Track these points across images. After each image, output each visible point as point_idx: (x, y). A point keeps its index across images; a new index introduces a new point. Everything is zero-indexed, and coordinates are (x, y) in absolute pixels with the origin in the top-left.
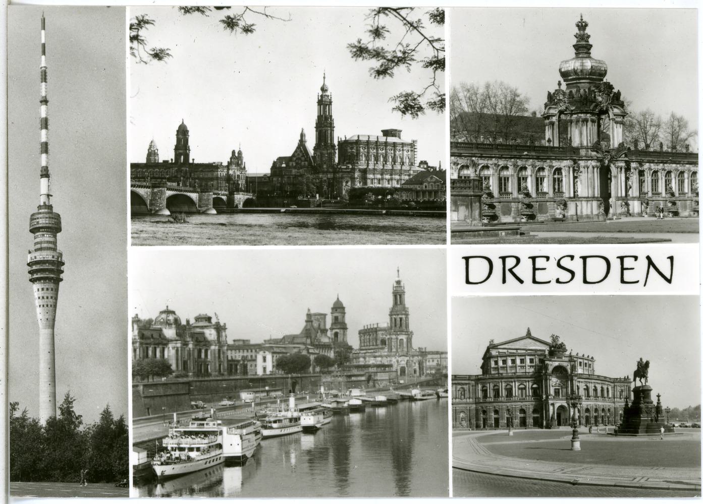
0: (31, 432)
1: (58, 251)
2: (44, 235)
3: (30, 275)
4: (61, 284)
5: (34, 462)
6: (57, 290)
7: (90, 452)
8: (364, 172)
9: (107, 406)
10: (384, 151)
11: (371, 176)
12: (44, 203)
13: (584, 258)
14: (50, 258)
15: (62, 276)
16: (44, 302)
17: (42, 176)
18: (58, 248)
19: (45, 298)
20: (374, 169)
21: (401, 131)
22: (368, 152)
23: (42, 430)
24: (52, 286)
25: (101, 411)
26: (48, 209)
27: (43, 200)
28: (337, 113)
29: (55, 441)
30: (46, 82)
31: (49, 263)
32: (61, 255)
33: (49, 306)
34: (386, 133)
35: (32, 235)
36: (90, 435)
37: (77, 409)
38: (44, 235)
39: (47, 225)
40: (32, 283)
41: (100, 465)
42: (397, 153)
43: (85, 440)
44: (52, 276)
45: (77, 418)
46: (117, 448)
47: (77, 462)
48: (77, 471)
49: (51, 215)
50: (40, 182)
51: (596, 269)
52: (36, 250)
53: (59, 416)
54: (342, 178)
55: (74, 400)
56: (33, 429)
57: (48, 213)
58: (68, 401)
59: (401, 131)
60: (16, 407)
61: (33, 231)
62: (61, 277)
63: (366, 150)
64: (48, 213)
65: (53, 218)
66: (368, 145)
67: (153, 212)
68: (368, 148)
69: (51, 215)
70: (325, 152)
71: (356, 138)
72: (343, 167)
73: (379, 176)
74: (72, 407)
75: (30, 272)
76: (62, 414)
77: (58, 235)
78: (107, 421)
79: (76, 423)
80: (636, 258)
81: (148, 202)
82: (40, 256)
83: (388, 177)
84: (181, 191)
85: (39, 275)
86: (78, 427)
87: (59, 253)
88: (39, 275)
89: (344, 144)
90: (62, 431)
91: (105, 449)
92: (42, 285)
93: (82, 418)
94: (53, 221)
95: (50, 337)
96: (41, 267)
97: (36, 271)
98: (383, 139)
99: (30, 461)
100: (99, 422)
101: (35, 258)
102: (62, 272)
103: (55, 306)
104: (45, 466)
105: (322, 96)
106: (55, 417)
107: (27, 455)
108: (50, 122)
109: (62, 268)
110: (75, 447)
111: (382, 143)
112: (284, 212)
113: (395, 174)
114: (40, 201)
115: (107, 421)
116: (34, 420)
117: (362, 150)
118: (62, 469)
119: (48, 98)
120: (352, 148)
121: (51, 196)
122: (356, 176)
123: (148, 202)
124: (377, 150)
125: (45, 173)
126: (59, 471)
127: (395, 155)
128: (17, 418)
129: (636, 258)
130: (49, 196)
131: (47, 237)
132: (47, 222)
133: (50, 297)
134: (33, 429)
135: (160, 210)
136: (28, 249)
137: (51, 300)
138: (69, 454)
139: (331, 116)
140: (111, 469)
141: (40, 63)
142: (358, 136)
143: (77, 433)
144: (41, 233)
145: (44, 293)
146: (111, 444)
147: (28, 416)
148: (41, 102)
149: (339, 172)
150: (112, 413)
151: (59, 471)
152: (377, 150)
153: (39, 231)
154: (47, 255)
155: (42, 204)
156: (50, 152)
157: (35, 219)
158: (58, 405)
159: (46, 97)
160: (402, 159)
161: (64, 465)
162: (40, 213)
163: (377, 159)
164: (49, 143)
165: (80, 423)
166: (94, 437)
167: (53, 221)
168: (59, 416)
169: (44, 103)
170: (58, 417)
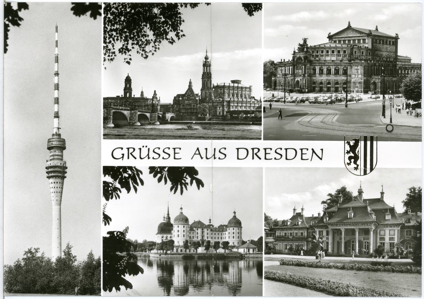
0: (47, 265)
1: (64, 161)
2: (55, 151)
3: (47, 174)
4: (65, 179)
5: (48, 282)
6: (63, 183)
7: (81, 277)
8: (229, 102)
9: (91, 251)
10: (237, 91)
11: (232, 104)
12: (56, 132)
13: (286, 149)
14: (59, 164)
15: (66, 175)
16: (56, 190)
17: (55, 117)
18: (64, 159)
19: (56, 187)
20: (234, 101)
21: (241, 81)
22: (229, 92)
23: (53, 264)
24: (59, 180)
25: (88, 253)
26: (58, 136)
27: (55, 131)
28: (214, 69)
29: (61, 270)
30: (58, 63)
31: (58, 168)
32: (65, 163)
33: (58, 192)
34: (233, 82)
35: (48, 151)
36: (81, 267)
37: (73, 252)
38: (55, 151)
39: (58, 145)
40: (48, 179)
41: (87, 285)
42: (243, 92)
43: (78, 270)
44: (60, 175)
45: (73, 258)
46: (97, 275)
47: (73, 283)
48: (73, 288)
49: (60, 140)
50: (53, 120)
51: (291, 154)
52: (51, 160)
53: (63, 256)
54: (217, 105)
55: (72, 247)
56: (48, 263)
57: (58, 138)
58: (69, 248)
59: (241, 81)
60: (38, 250)
61: (49, 148)
62: (65, 176)
63: (228, 91)
64: (58, 138)
65: (61, 141)
66: (229, 88)
67: (131, 124)
68: (229, 90)
69: (60, 140)
70: (207, 92)
71: (223, 85)
72: (217, 100)
73: (236, 105)
74: (71, 251)
75: (47, 173)
76: (65, 255)
77: (64, 151)
78: (91, 260)
79: (73, 260)
80: (307, 149)
81: (128, 119)
82: (52, 163)
83: (240, 105)
84: (143, 112)
85: (52, 174)
86: (74, 262)
87: (65, 162)
88: (52, 174)
89: (218, 87)
90: (65, 265)
91: (90, 275)
92: (54, 180)
93: (76, 257)
94: (61, 143)
95: (58, 210)
96: (54, 170)
97: (51, 172)
98: (232, 85)
99: (46, 282)
100: (86, 260)
101: (50, 164)
102: (66, 173)
103: (62, 193)
104: (55, 285)
105: (205, 62)
106: (61, 257)
107: (44, 278)
108: (60, 86)
109: (66, 170)
110: (72, 274)
111: (236, 87)
112: (195, 123)
113: (244, 103)
114: (53, 132)
115: (91, 260)
116: (48, 258)
117: (226, 91)
118: (64, 287)
119: (59, 72)
120: (221, 90)
121: (60, 128)
122: (225, 104)
123: (128, 119)
124: (233, 91)
125: (57, 116)
126: (62, 288)
127: (242, 93)
128: (39, 257)
129: (307, 149)
130: (59, 128)
131: (58, 153)
132: (58, 143)
133: (58, 187)
134: (48, 263)
135: (135, 123)
136: (46, 159)
137: (59, 189)
138: (69, 278)
139: (210, 72)
140: (93, 287)
141: (55, 52)
142: (224, 83)
143: (74, 266)
144: (54, 150)
145: (55, 185)
146: (93, 273)
147: (45, 256)
148: (55, 74)
149: (215, 102)
150: (94, 255)
151: (62, 288)
152: (233, 91)
153: (53, 149)
154: (57, 163)
155: (55, 133)
156: (60, 103)
157: (51, 142)
158: (63, 250)
159: (58, 71)
160: (245, 95)
161: (66, 284)
162: (54, 138)
163: (233, 96)
164: (60, 98)
165: (75, 260)
166: (83, 268)
167: (61, 143)
168: (63, 256)
169: (57, 75)
170: (62, 257)
